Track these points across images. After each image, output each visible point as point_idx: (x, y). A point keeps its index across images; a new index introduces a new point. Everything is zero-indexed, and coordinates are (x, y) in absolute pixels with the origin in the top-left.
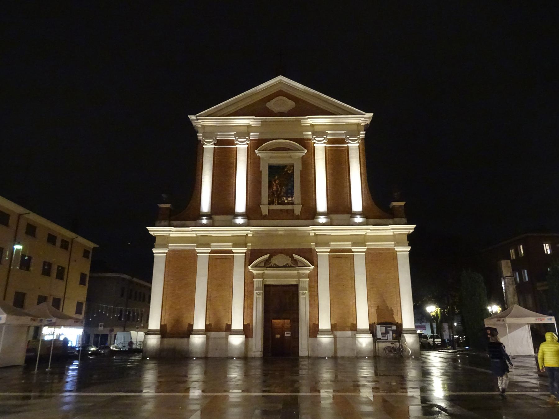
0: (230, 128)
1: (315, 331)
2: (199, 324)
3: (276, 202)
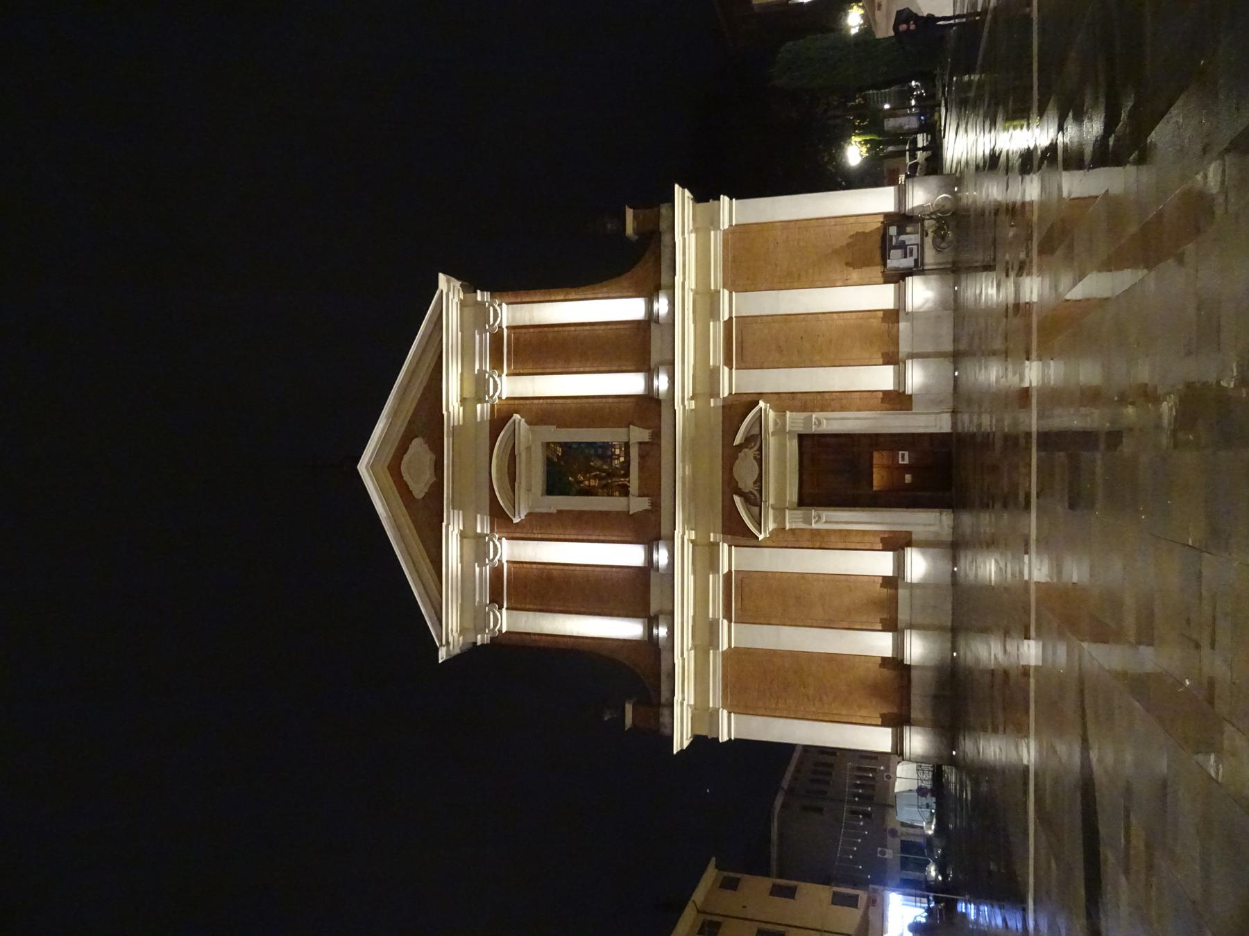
0: (466, 577)
1: (897, 400)
2: (880, 644)
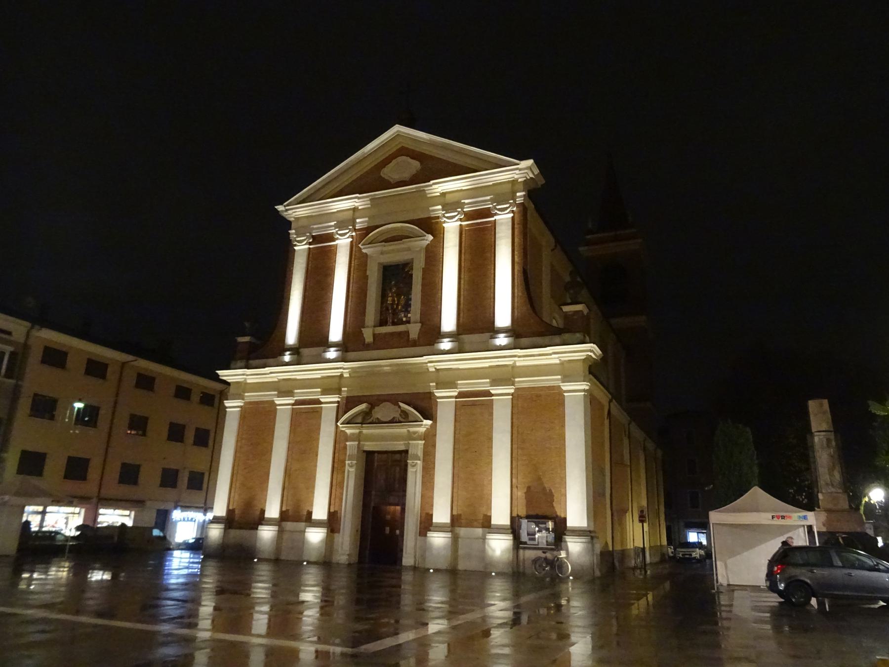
0: (329, 216)
1: (427, 524)
2: (273, 511)
3: (390, 320)
